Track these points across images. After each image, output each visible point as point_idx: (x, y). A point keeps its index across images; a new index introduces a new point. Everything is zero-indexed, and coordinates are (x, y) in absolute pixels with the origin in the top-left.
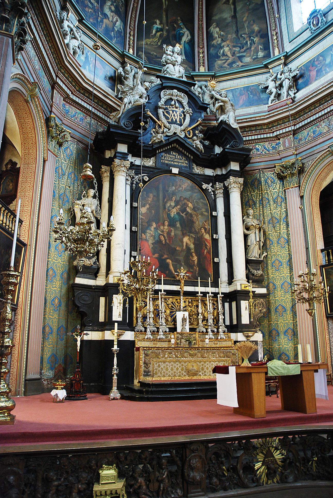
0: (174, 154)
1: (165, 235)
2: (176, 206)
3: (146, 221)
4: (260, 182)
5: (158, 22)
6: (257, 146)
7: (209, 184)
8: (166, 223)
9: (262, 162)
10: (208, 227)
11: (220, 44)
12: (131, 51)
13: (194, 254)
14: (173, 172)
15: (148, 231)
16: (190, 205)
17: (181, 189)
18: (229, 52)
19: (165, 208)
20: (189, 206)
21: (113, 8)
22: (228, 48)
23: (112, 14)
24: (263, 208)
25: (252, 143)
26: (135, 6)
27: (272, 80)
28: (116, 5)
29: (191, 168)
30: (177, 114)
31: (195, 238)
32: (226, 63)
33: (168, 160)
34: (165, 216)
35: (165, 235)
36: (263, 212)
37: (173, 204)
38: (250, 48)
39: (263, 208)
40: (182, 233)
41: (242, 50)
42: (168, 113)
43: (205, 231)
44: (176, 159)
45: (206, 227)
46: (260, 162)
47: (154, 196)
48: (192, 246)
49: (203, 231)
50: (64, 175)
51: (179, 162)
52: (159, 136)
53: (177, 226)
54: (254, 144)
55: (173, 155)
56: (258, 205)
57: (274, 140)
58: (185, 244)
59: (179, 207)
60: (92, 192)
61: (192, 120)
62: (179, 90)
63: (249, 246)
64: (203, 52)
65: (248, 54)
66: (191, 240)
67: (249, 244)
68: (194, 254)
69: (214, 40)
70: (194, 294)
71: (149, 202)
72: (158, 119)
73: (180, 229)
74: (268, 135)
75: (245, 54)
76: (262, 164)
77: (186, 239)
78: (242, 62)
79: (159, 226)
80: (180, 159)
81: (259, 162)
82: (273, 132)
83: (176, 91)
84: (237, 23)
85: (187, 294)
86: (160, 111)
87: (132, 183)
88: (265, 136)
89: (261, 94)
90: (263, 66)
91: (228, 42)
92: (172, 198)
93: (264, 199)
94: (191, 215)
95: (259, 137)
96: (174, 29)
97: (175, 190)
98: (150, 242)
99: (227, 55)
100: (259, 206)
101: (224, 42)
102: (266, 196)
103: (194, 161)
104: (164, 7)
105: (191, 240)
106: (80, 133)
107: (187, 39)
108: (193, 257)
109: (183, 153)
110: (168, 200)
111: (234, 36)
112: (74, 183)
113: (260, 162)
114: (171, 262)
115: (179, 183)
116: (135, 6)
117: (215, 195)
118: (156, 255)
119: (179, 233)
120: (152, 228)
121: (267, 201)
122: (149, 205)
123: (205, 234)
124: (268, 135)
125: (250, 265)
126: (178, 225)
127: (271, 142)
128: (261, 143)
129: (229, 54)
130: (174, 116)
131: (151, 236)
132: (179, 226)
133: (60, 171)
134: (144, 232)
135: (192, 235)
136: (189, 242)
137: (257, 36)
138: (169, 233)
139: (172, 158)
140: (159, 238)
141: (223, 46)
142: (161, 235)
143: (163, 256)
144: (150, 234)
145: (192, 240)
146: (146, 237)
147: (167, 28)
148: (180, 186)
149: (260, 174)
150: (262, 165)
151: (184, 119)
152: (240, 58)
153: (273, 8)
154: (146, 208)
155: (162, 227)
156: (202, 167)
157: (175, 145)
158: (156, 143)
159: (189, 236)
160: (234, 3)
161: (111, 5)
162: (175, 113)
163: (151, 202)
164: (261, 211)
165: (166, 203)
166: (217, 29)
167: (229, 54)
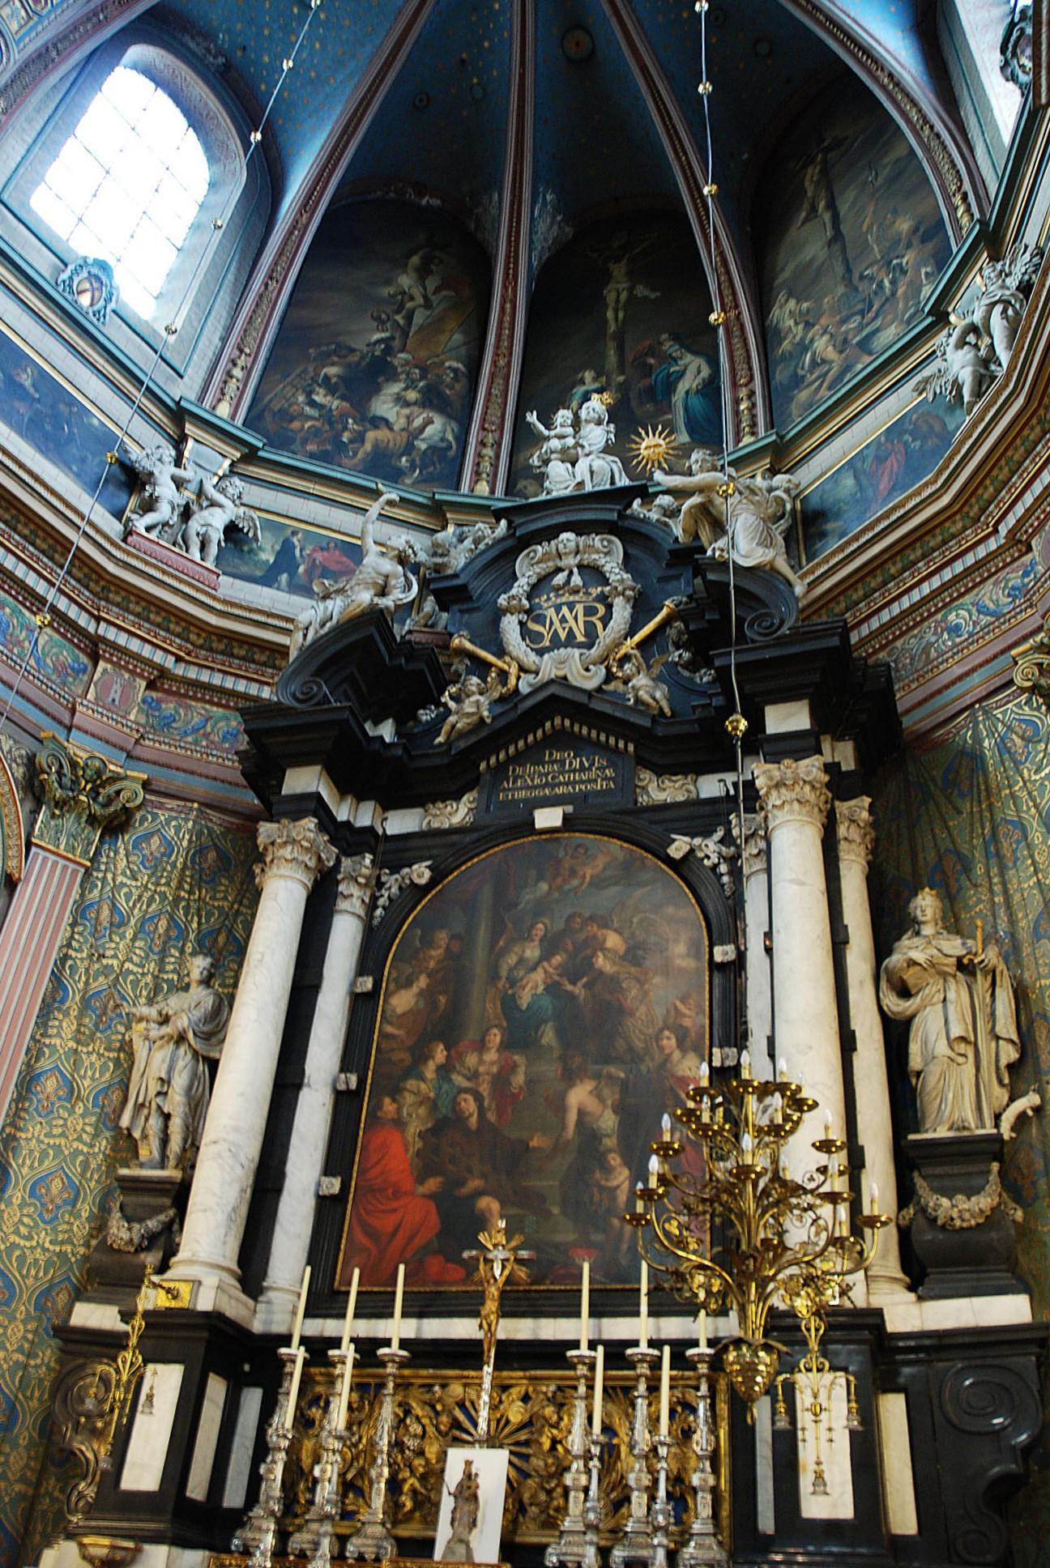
0: (557, 755)
1: (485, 1089)
2: (546, 956)
3: (409, 1043)
4: (975, 758)
5: (588, 375)
6: (952, 617)
7: (707, 833)
8: (496, 1037)
9: (974, 670)
10: (696, 1019)
11: (803, 339)
12: (483, 488)
13: (615, 1160)
14: (538, 825)
15: (411, 1084)
16: (613, 940)
17: (575, 882)
18: (830, 348)
19: (494, 976)
20: (609, 944)
21: (412, 395)
22: (826, 338)
23: (406, 411)
24: (1002, 874)
25: (931, 615)
26: (502, 363)
27: (962, 343)
28: (427, 386)
29: (628, 786)
30: (565, 616)
31: (624, 1086)
32: (825, 385)
33: (528, 788)
34: (492, 1008)
35: (485, 1089)
36: (1006, 892)
37: (532, 952)
38: (893, 294)
39: (1002, 874)
40: (564, 1069)
41: (871, 315)
42: (540, 619)
43: (681, 1044)
44: (562, 773)
45: (687, 1022)
46: (967, 674)
47: (453, 937)
48: (608, 1121)
49: (670, 1042)
50: (123, 923)
51: (575, 782)
52: (468, 707)
53: (545, 1040)
54: (939, 616)
55: (556, 761)
56: (980, 869)
57: (1014, 560)
58: (572, 1117)
59: (558, 959)
60: (198, 965)
61: (642, 608)
62: (580, 529)
63: (918, 1074)
64: (752, 394)
65: (890, 317)
66: (606, 1092)
67: (915, 1061)
68: (615, 1160)
69: (785, 338)
70: (554, 1354)
71: (432, 964)
72: (501, 652)
73: (556, 1053)
74: (981, 551)
75: (878, 322)
76: (976, 678)
77: (579, 1096)
78: (870, 354)
79: (461, 1056)
80: (582, 769)
81: (960, 678)
82: (996, 531)
83: (567, 536)
84: (844, 250)
85: (513, 1354)
86: (510, 626)
87: (372, 906)
88: (970, 559)
89: (947, 419)
90: (930, 320)
91: (823, 321)
92: (533, 926)
93: (1002, 830)
94: (614, 982)
95: (947, 574)
96: (648, 371)
97: (549, 892)
98: (414, 1128)
99: (824, 361)
100: (988, 871)
101: (813, 325)
102: (1011, 813)
103: (642, 762)
104: (612, 328)
105: (606, 1092)
106: (215, 779)
107: (699, 380)
108: (608, 1170)
109: (597, 744)
110: (511, 942)
111: (841, 290)
112: (163, 951)
113: (967, 674)
114: (495, 1206)
115: (567, 863)
116: (502, 363)
117: (736, 874)
118: (433, 1184)
119: (550, 1070)
120: (430, 1070)
121: (1017, 835)
122: (429, 976)
123: (677, 1055)
124: (981, 551)
125: (929, 1171)
126: (548, 1036)
127: (1002, 574)
128: (968, 599)
129: (831, 353)
130: (563, 620)
131: (421, 1103)
132: (554, 1043)
133: (105, 912)
134: (395, 1093)
135: (612, 1070)
136: (592, 1105)
137: (909, 246)
138: (501, 1081)
139: (546, 775)
140: (455, 1103)
141: (812, 341)
142: (466, 1091)
143: (463, 1184)
144: (417, 1093)
145: (611, 1095)
146: (399, 1110)
147: (621, 378)
148: (573, 873)
149: (976, 724)
150: (977, 684)
151: (606, 620)
152: (864, 346)
153: (938, 136)
154: (415, 989)
155: (471, 1060)
156: (685, 774)
157: (567, 723)
158: (463, 735)
159: (597, 1076)
160: (832, 206)
161: (406, 389)
162: (565, 610)
163: (438, 962)
164: (997, 888)
165: (503, 953)
166: (792, 304)
167: (831, 353)
